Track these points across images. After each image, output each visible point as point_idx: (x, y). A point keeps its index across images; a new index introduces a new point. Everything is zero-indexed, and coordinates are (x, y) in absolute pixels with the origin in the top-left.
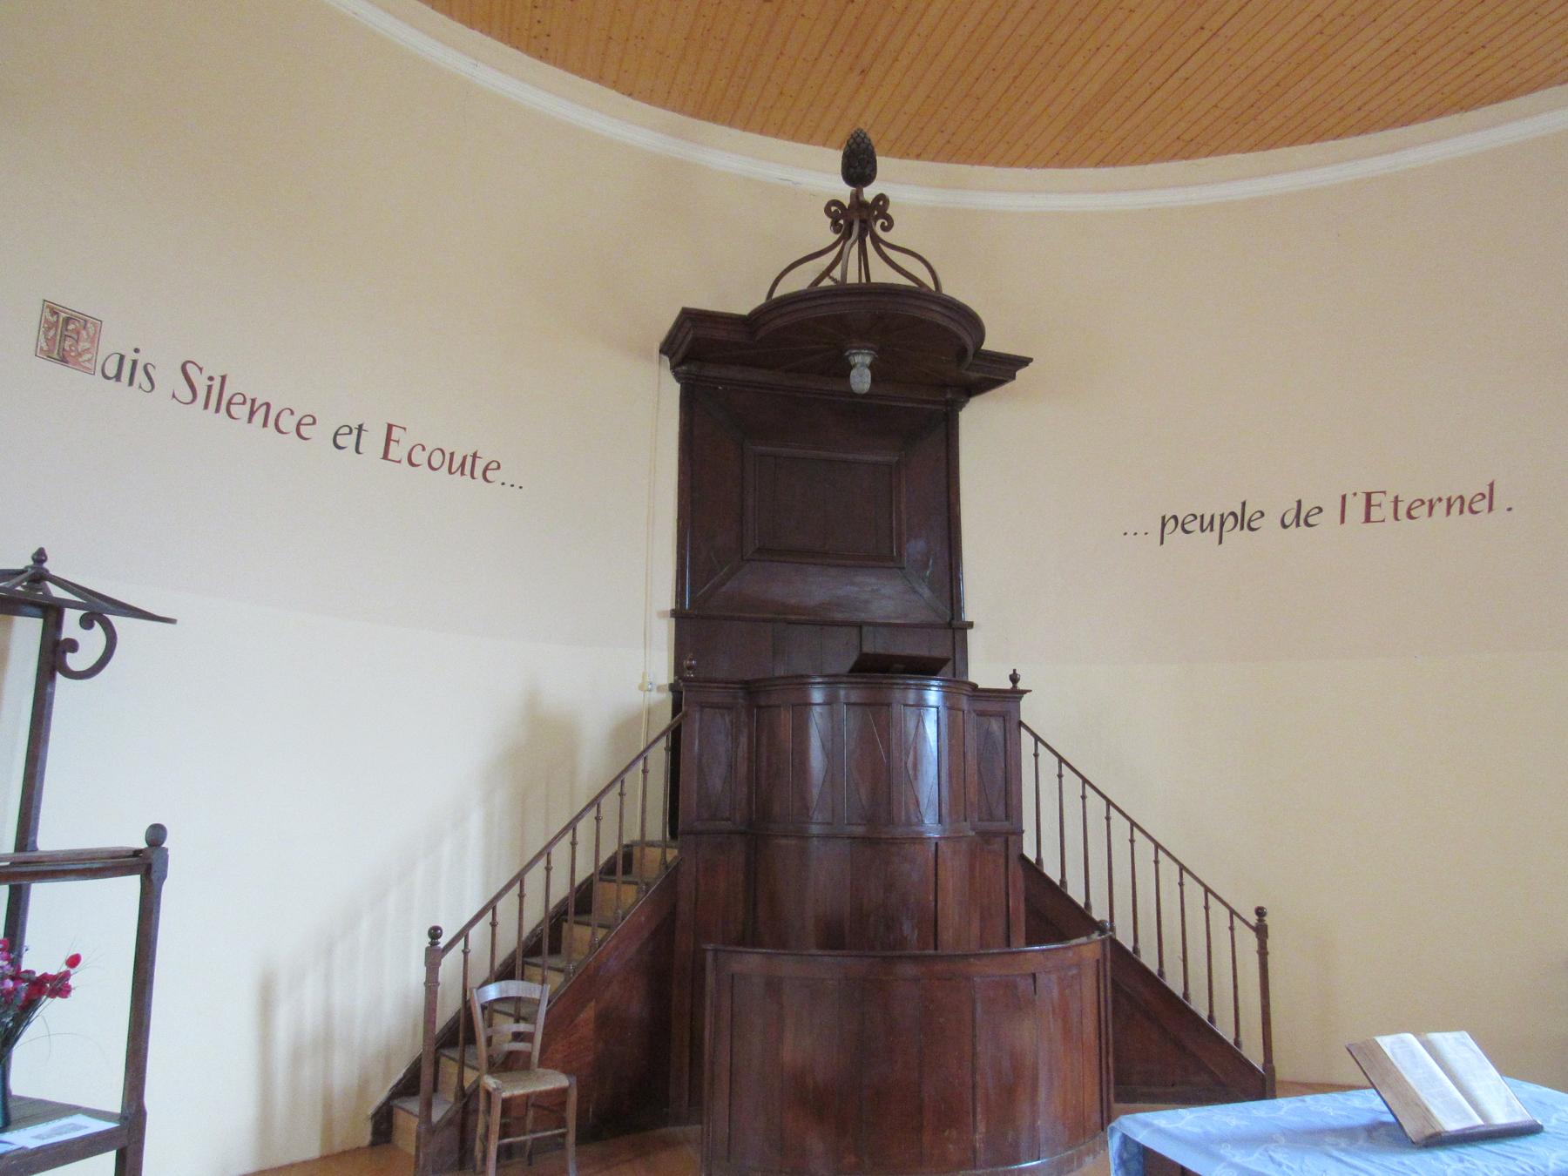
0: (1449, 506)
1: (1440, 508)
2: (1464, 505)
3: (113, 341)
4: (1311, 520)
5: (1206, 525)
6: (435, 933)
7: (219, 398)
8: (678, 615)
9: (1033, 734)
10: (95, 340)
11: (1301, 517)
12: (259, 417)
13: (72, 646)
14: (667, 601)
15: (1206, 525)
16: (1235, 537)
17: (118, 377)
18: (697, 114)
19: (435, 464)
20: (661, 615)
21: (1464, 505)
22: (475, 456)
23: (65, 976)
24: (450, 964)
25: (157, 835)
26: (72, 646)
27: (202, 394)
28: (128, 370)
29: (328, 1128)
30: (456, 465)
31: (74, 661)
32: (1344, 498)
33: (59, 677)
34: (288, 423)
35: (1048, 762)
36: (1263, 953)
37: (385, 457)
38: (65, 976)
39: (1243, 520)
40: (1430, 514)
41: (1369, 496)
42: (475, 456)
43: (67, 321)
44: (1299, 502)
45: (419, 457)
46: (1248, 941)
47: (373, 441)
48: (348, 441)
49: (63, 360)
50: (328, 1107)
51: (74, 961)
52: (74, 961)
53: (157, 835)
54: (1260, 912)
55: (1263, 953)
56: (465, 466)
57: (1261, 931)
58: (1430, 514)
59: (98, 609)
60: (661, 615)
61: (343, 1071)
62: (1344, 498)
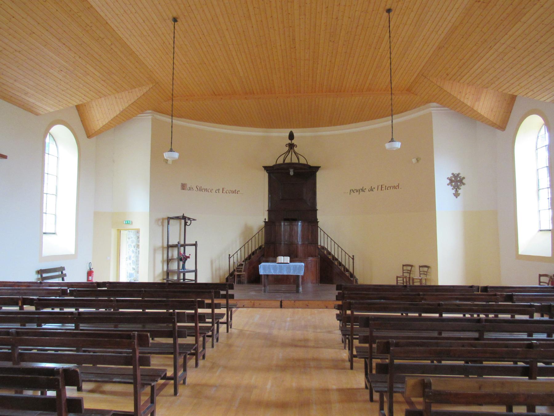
0: (393, 187)
1: (392, 188)
2: (394, 187)
3: (188, 186)
4: (373, 190)
5: (357, 191)
6: (229, 255)
7: (201, 189)
8: (268, 211)
9: (320, 228)
10: (187, 186)
11: (372, 190)
12: (206, 191)
13: (187, 222)
14: (267, 209)
15: (357, 191)
16: (361, 193)
17: (189, 190)
18: (268, 128)
19: (230, 192)
20: (266, 211)
21: (394, 187)
22: (235, 190)
23: (189, 256)
24: (232, 259)
25: (196, 242)
26: (187, 222)
27: (199, 189)
28: (190, 189)
29: (220, 279)
30: (233, 192)
31: (188, 224)
32: (378, 186)
33: (186, 226)
34: (209, 191)
35: (322, 233)
36: (353, 262)
37: (223, 192)
38: (189, 256)
39: (363, 190)
40: (390, 189)
41: (382, 186)
42: (235, 190)
43: (184, 185)
44: (371, 187)
45: (227, 192)
46: (351, 260)
47: (221, 191)
48: (217, 191)
49: (184, 189)
50: (220, 277)
51: (190, 255)
52: (190, 255)
53: (196, 242)
54: (353, 256)
55: (353, 262)
56: (234, 192)
57: (353, 259)
58: (390, 189)
59: (189, 219)
60: (266, 211)
61: (222, 273)
62: (378, 186)
